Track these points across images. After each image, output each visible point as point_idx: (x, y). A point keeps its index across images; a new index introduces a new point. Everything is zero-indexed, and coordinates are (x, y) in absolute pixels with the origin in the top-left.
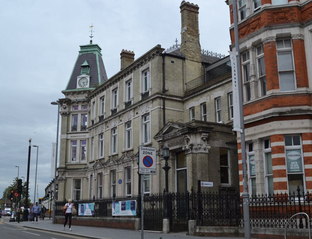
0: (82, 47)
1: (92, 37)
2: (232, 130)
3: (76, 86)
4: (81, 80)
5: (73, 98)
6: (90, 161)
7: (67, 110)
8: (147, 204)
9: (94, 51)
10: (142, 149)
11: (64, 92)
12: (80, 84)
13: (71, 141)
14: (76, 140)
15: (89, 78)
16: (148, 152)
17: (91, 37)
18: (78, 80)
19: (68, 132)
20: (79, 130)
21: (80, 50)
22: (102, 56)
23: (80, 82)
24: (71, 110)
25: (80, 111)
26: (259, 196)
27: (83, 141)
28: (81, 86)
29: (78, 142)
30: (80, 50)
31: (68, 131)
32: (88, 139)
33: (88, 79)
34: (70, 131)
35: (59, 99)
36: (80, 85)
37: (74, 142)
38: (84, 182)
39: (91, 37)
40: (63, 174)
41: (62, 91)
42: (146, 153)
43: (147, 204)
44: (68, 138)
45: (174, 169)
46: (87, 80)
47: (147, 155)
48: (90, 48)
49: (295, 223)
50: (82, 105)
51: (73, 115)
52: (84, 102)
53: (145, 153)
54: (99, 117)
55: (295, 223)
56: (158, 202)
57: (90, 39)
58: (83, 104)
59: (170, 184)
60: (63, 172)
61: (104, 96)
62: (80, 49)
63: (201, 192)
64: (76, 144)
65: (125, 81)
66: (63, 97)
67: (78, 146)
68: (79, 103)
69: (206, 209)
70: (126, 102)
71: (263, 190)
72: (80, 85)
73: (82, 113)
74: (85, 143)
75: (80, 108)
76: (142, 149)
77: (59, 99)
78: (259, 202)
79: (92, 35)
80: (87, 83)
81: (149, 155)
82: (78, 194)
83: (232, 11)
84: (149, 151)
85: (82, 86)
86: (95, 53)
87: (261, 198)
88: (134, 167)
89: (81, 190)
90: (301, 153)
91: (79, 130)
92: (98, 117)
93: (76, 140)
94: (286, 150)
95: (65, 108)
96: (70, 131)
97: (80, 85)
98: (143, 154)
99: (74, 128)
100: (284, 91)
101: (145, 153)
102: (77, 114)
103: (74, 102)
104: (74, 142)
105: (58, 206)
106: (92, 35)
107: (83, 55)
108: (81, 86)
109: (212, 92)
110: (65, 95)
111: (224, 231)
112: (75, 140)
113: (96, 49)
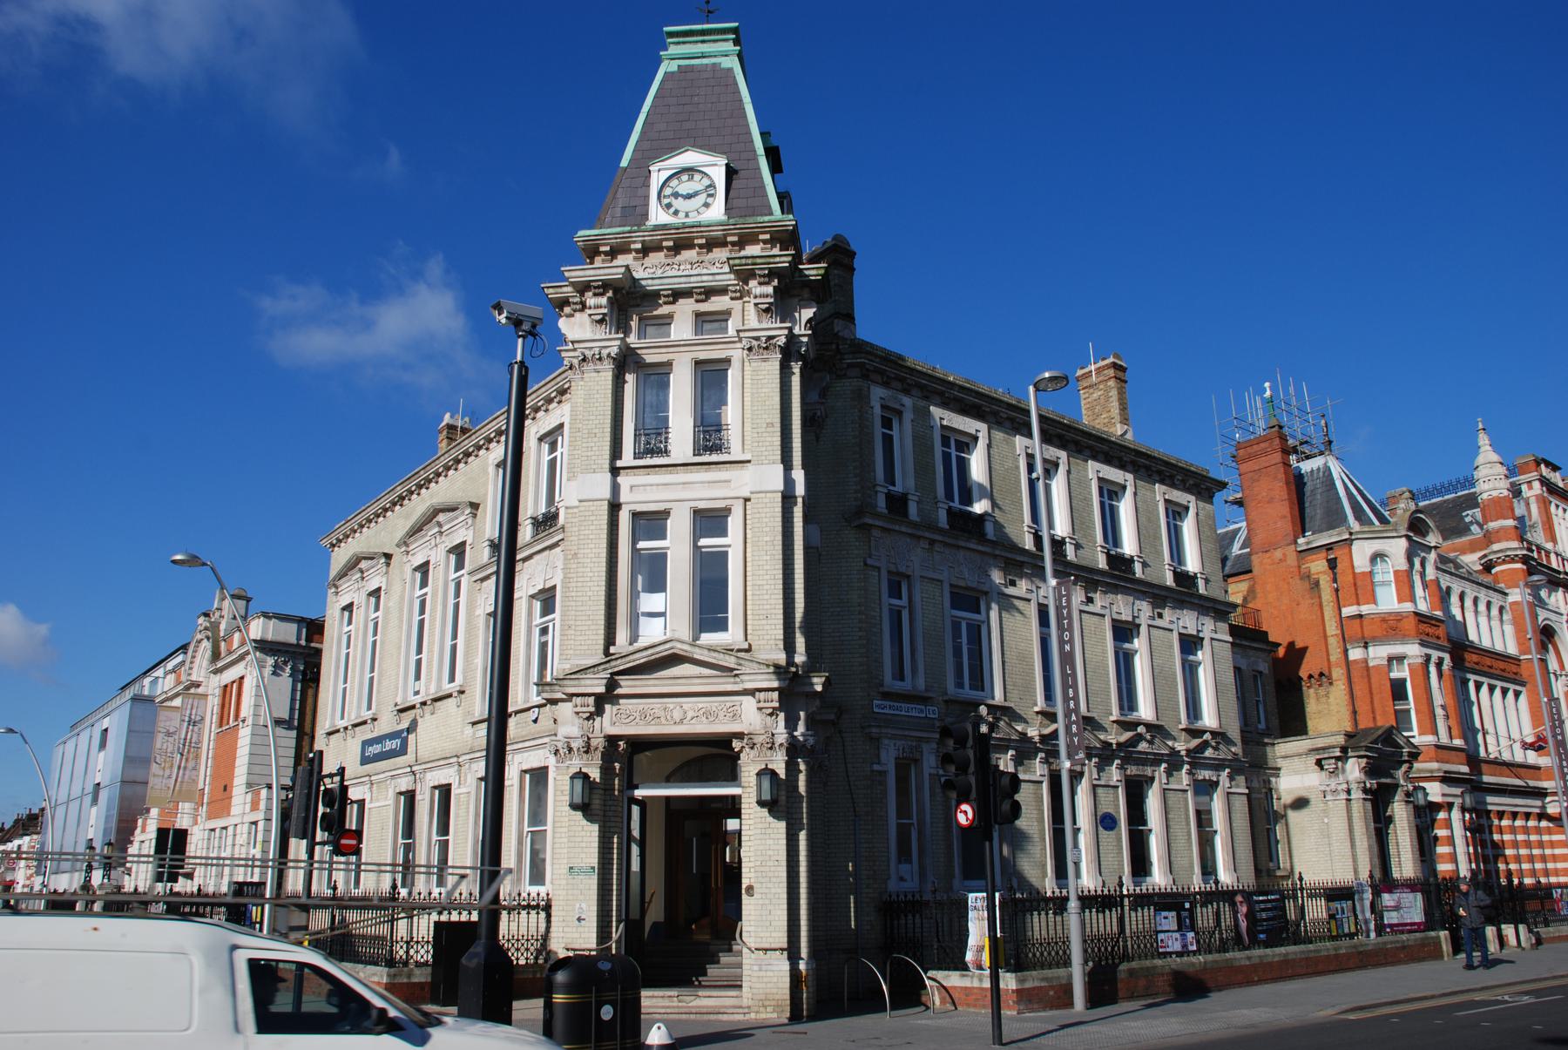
3: (646, 216)
6: (476, 715)
15: (723, 169)
18: (656, 180)
26: (420, 894)
27: (710, 520)
28: (672, 210)
32: (747, 500)
33: (719, 175)
46: (712, 186)
54: (534, 518)
58: (704, 307)
59: (1488, 704)
61: (561, 426)
65: (538, 435)
68: (681, 301)
70: (535, 516)
75: (682, 328)
80: (710, 200)
82: (537, 847)
85: (681, 215)
88: (459, 787)
89: (549, 827)
92: (529, 521)
94: (1005, 700)
108: (672, 210)
111: (1020, 981)
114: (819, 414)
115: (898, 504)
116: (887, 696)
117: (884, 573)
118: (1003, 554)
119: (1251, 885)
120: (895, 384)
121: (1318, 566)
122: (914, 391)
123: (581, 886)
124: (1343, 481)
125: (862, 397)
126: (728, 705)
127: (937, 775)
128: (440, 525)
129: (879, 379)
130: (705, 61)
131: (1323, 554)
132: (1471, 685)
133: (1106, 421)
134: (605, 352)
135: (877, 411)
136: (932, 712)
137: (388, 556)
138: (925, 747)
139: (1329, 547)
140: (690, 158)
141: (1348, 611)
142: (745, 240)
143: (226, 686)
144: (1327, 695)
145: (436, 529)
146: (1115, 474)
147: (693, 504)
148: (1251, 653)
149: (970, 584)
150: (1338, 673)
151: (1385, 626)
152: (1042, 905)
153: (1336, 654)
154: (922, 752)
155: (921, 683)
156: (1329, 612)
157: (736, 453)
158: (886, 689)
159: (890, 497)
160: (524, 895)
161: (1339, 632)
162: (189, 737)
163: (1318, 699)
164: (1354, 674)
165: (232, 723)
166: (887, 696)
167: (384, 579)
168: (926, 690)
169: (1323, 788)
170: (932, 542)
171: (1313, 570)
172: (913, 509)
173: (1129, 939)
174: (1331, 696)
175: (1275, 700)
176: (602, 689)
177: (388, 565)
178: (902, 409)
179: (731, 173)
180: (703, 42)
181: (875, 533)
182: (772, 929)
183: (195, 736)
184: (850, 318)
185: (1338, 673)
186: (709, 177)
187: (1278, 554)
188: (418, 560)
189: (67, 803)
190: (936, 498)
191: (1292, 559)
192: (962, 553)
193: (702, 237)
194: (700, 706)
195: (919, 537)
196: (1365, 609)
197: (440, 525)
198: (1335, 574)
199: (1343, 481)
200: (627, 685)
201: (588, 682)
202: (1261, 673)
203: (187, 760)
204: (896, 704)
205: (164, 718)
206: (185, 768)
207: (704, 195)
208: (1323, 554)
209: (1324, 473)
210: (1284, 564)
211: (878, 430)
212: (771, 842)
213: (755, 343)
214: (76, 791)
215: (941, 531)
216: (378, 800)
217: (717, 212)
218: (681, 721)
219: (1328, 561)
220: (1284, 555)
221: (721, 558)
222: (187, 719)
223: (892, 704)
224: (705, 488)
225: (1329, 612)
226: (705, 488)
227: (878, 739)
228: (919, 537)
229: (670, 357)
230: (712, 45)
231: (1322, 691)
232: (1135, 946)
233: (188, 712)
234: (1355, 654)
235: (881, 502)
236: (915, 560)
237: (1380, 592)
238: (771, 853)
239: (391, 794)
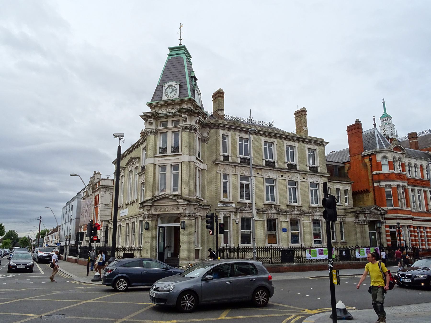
0: (171, 49)
1: (182, 39)
2: (390, 272)
4: (168, 89)
5: (162, 112)
7: (154, 126)
9: (182, 54)
11: (150, 105)
12: (166, 94)
13: (159, 166)
14: (166, 166)
17: (179, 40)
18: (164, 89)
19: (156, 155)
20: (169, 151)
21: (169, 52)
22: (192, 65)
23: (167, 91)
24: (159, 127)
25: (170, 128)
27: (175, 167)
28: (168, 96)
29: (168, 168)
30: (169, 52)
31: (155, 153)
33: (177, 87)
34: (158, 154)
35: (143, 113)
36: (167, 95)
37: (163, 168)
38: (349, 194)
39: (180, 40)
40: (150, 210)
41: (146, 103)
44: (155, 163)
46: (176, 89)
50: (173, 121)
51: (161, 133)
52: (173, 116)
60: (149, 207)
62: (169, 52)
64: (165, 170)
66: (149, 110)
67: (169, 172)
68: (169, 118)
72: (166, 95)
73: (173, 130)
74: (177, 169)
77: (143, 113)
80: (176, 93)
85: (170, 97)
86: (182, 56)
90: (265, 266)
91: (169, 151)
93: (166, 166)
95: (151, 124)
96: (158, 154)
97: (167, 95)
99: (163, 150)
102: (167, 132)
103: (163, 117)
104: (163, 168)
105: (380, 183)
106: (180, 37)
107: (172, 58)
108: (168, 96)
109: (335, 184)
110: (151, 108)
112: (165, 165)
113: (183, 51)
114: (206, 138)
115: (226, 158)
116: (221, 202)
117: (222, 174)
118: (255, 167)
119: (237, 247)
120: (226, 129)
121: (367, 160)
122: (232, 130)
123: (147, 246)
124: (378, 135)
125: (217, 134)
126: (177, 207)
127: (235, 220)
128: (133, 162)
129: (222, 128)
130: (177, 56)
131: (368, 157)
132: (410, 191)
133: (301, 126)
134: (152, 131)
135: (221, 136)
136: (234, 205)
137: (125, 168)
138: (231, 213)
139: (370, 155)
140: (171, 83)
141: (374, 173)
142: (183, 102)
143: (96, 196)
144: (368, 195)
145: (132, 163)
146: (292, 143)
147: (171, 164)
148: (344, 184)
149: (245, 175)
150: (371, 190)
151: (385, 177)
152: (243, 250)
153: (371, 185)
154: (231, 215)
155: (231, 199)
156: (369, 173)
157: (180, 153)
158: (221, 201)
159: (224, 156)
160: (133, 247)
161: (371, 178)
162: (88, 209)
163: (366, 196)
164: (376, 190)
165: (97, 205)
166: (221, 202)
167: (124, 173)
168: (232, 201)
169: (355, 221)
170: (235, 166)
171: (366, 161)
172: (230, 159)
173: (303, 258)
174: (369, 195)
175: (352, 197)
176: (151, 205)
177: (125, 170)
178: (228, 135)
179: (180, 87)
180: (177, 50)
181: (219, 165)
182: (184, 255)
183: (89, 208)
184: (222, 110)
185: (371, 190)
186: (176, 88)
187: (357, 157)
188: (130, 170)
189: (66, 223)
190: (237, 155)
191: (360, 158)
192: (243, 168)
193: (173, 103)
194: (171, 207)
195: (231, 165)
196: (380, 172)
197: (133, 162)
198: (371, 162)
199: (378, 135)
200: (156, 203)
201: (148, 203)
202: (347, 190)
203: (87, 214)
204: (224, 204)
205: (89, 201)
206: (87, 216)
207: (175, 92)
208: (368, 157)
209: (373, 133)
210: (358, 159)
211: (221, 140)
212: (184, 236)
213: (183, 128)
214: (67, 221)
215: (239, 164)
216: (123, 225)
217: (177, 96)
218: (167, 211)
219: (369, 159)
220: (358, 157)
221: (177, 174)
222: (87, 204)
223: (223, 204)
224: (173, 160)
225: (369, 173)
226: (173, 160)
227: (219, 212)
228: (231, 165)
229: (167, 131)
230: (179, 51)
231: (367, 194)
232: (275, 260)
233: (87, 202)
234: (376, 184)
235: (222, 158)
236: (230, 170)
237: (383, 167)
238: (184, 239)
239: (125, 224)
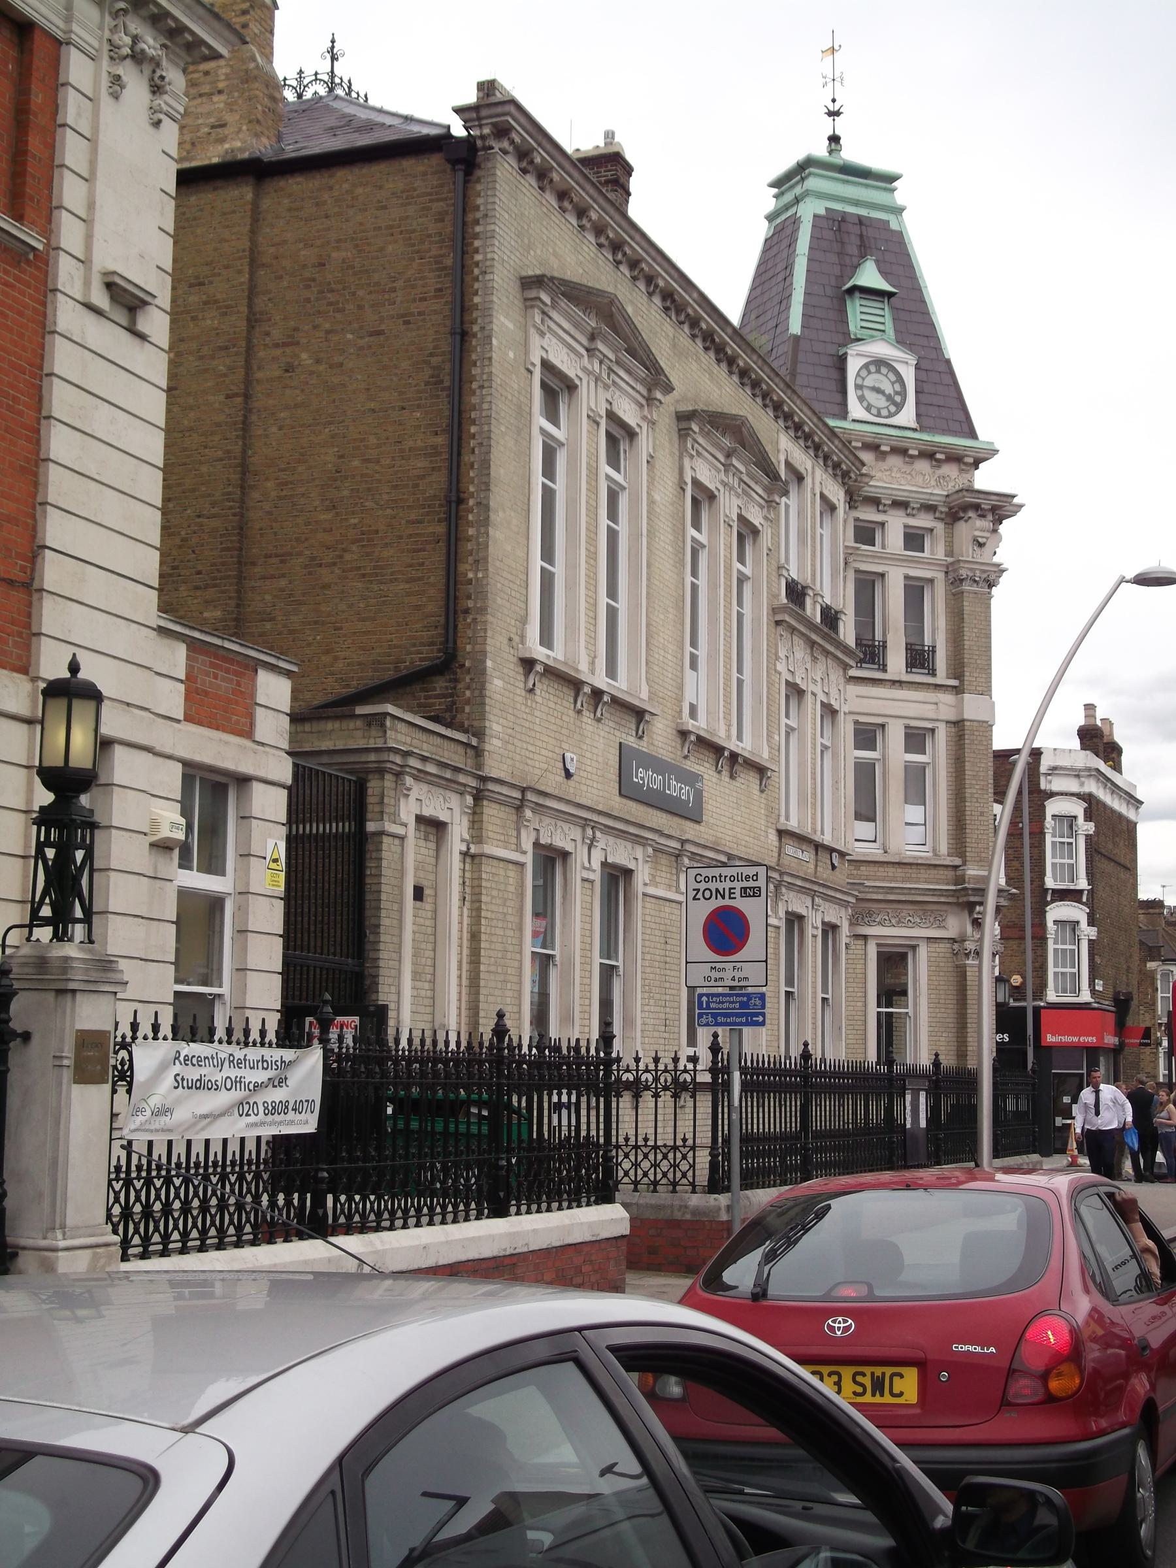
8: (593, 1126)
10: (699, 878)
16: (717, 890)
42: (707, 894)
43: (593, 1126)
45: (588, 981)
47: (721, 902)
48: (118, 1526)
49: (690, 1174)
53: (700, 895)
55: (690, 1174)
56: (565, 1091)
57: (826, 127)
63: (619, 1060)
64: (908, 767)
69: (646, 1140)
71: (432, 1001)
76: (699, 878)
78: (656, 1088)
79: (834, 101)
81: (727, 902)
83: (745, 322)
84: (721, 886)
87: (666, 1071)
98: (694, 899)
100: (29, 1398)
101: (700, 895)
106: (834, 101)
